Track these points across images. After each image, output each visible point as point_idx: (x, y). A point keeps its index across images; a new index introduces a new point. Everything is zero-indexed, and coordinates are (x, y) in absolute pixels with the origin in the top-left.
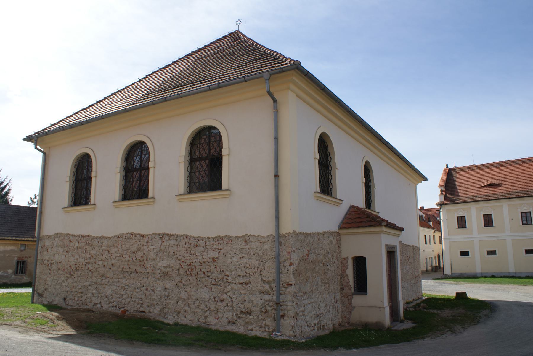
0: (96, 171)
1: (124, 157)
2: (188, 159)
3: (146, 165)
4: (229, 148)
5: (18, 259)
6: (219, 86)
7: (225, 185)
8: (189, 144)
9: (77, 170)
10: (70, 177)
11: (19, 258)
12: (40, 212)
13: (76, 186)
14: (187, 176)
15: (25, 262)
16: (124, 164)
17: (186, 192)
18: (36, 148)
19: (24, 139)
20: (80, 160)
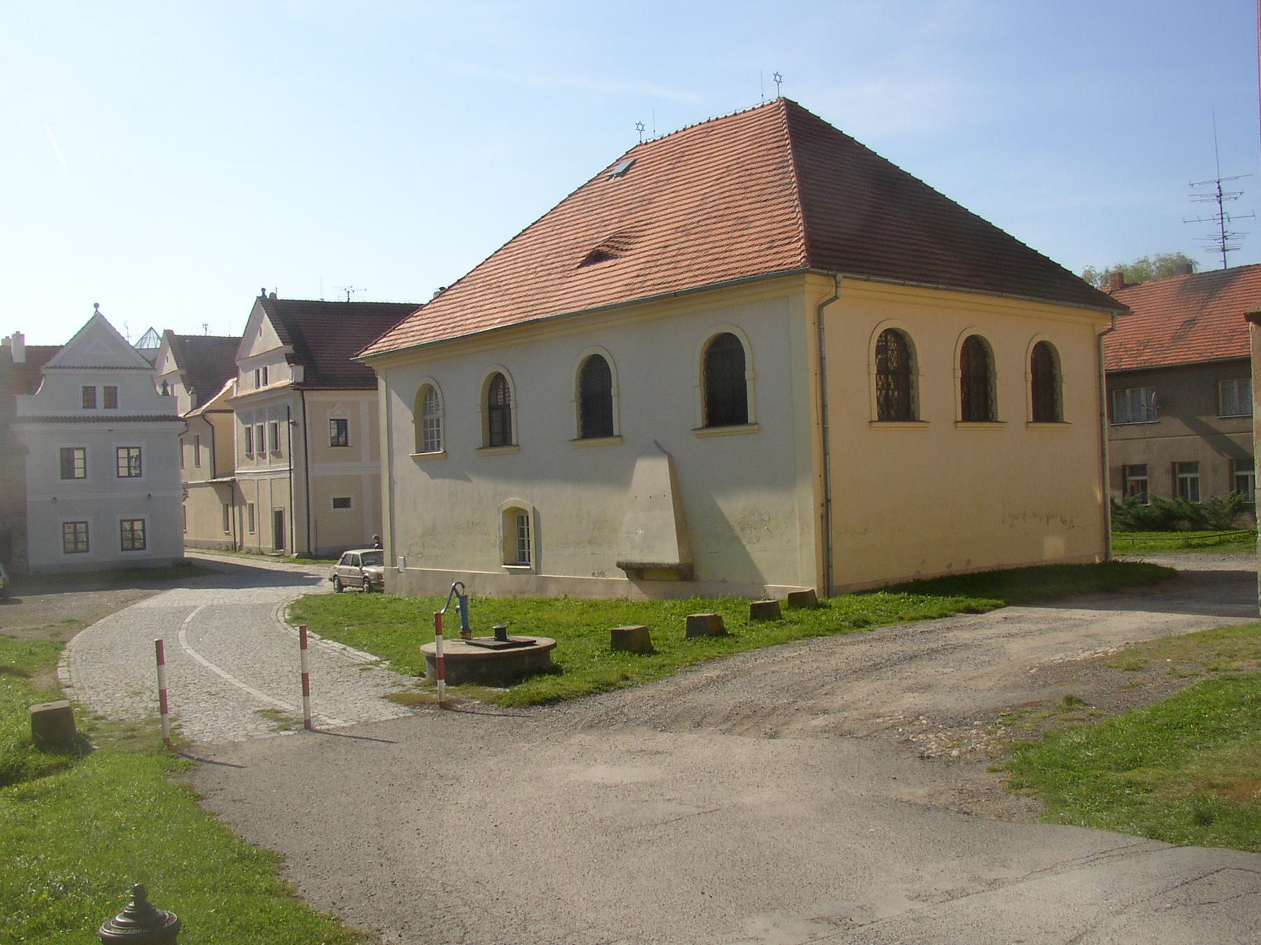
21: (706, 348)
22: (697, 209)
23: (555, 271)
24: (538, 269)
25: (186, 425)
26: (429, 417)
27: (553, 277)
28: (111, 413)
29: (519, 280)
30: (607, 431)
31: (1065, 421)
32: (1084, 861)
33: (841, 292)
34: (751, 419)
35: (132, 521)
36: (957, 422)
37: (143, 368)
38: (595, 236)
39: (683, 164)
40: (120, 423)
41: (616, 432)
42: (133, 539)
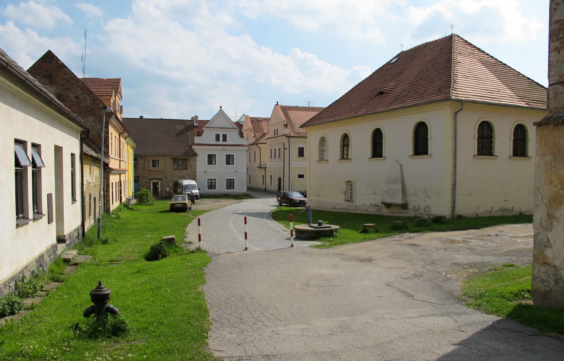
0: (351, 144)
21: (415, 127)
22: (417, 76)
23: (367, 98)
24: (362, 97)
25: (249, 148)
26: (323, 148)
27: (366, 100)
28: (224, 143)
29: (355, 101)
30: (380, 155)
31: (529, 156)
32: (252, 358)
33: (464, 107)
34: (429, 153)
35: (211, 180)
36: (510, 156)
37: (235, 128)
38: (382, 86)
39: (415, 59)
40: (212, 147)
41: (383, 156)
42: (211, 186)
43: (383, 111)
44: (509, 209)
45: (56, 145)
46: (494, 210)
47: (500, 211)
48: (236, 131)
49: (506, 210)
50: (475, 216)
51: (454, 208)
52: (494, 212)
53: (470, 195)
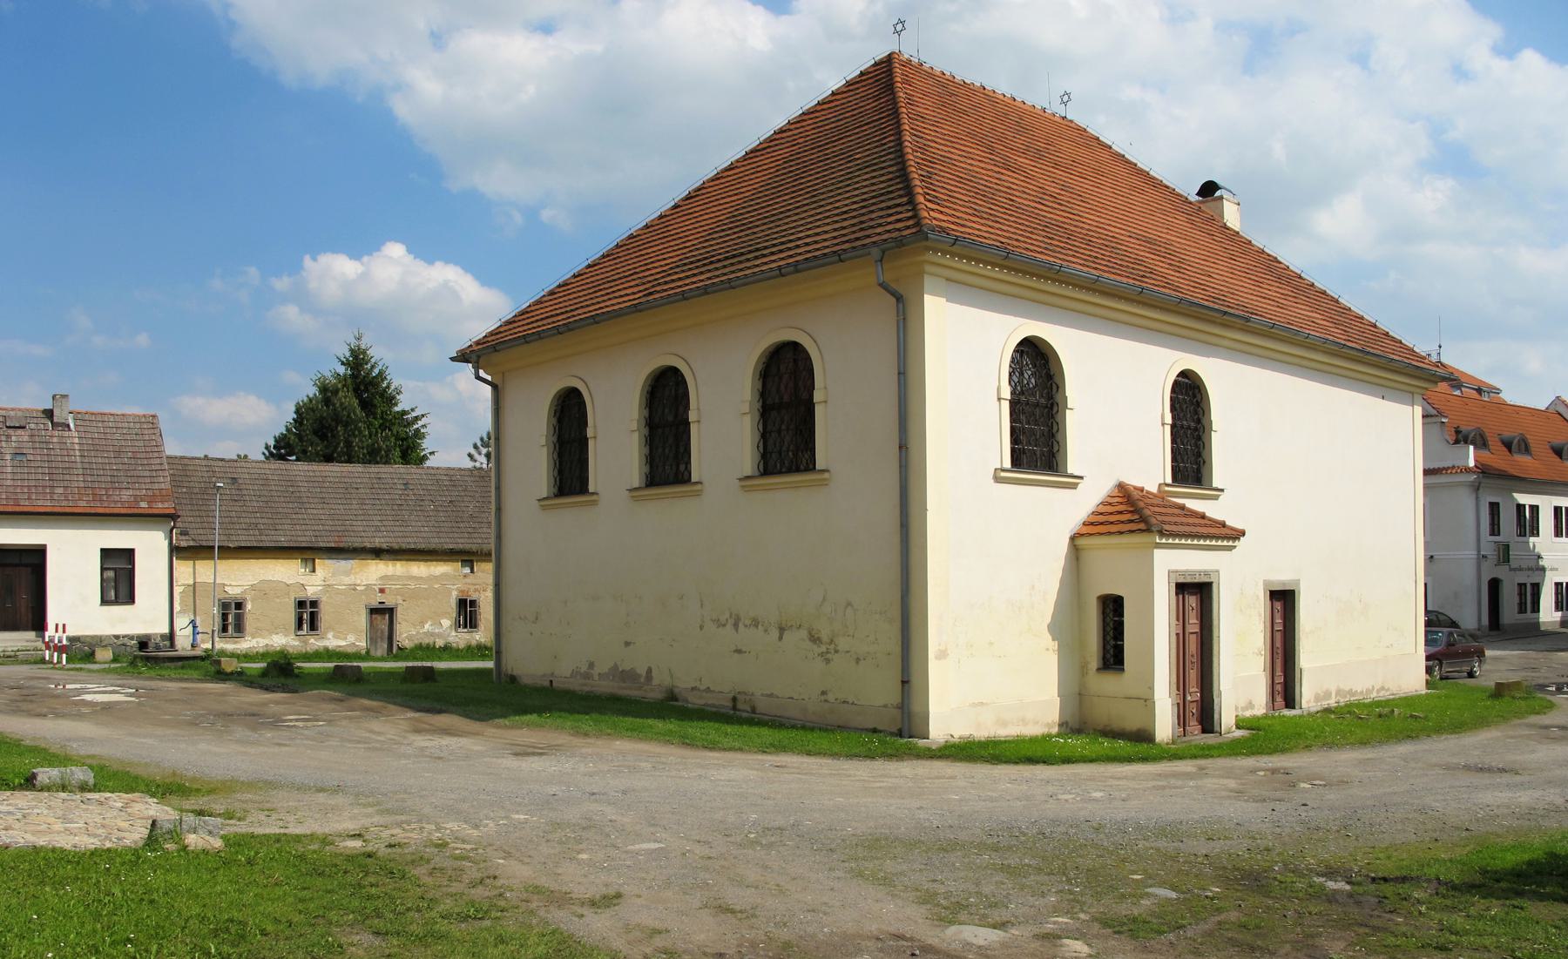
0: (595, 426)
1: (645, 400)
2: (758, 405)
3: (685, 417)
4: (825, 388)
5: (460, 594)
6: (797, 268)
7: (821, 461)
8: (758, 377)
9: (560, 421)
10: (547, 436)
11: (462, 591)
12: (496, 509)
13: (560, 455)
14: (757, 440)
15: (475, 601)
16: (646, 413)
17: (757, 473)
18: (478, 377)
19: (453, 359)
20: (564, 401)
37: (1432, 416)
43: (1559, 520)
44: (640, 676)
45: (1269, 581)
46: (596, 672)
47: (611, 678)
48: (1460, 484)
49: (628, 676)
50: (547, 684)
51: (194, 564)
52: (596, 678)
53: (537, 619)
